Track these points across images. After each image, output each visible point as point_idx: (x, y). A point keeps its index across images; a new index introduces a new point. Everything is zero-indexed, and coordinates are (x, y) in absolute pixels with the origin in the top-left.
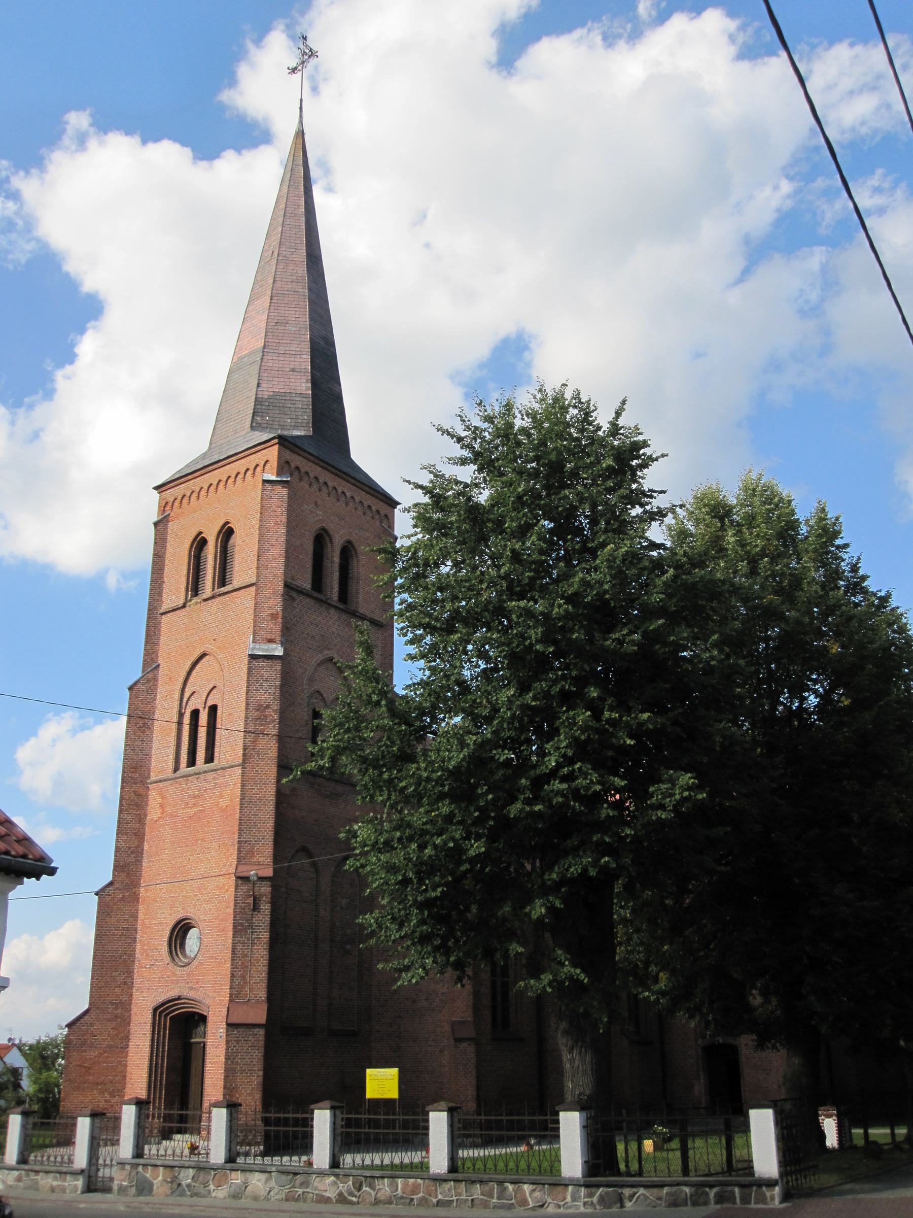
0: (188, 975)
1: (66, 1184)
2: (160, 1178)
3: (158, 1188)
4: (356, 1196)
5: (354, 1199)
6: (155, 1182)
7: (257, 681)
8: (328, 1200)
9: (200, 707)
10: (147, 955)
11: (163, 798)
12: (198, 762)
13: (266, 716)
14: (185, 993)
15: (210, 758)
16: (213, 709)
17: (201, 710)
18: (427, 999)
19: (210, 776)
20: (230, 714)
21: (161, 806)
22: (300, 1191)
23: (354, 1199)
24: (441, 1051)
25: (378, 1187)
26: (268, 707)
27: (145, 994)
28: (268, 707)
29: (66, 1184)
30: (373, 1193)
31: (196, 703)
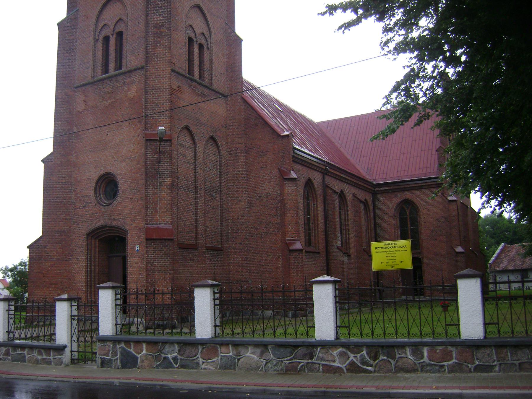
0: (111, 211)
1: (51, 358)
2: (144, 352)
3: (142, 361)
4: (371, 366)
5: (369, 368)
6: (139, 356)
7: (154, 8)
8: (337, 370)
9: (109, 34)
10: (80, 200)
11: (86, 96)
12: (110, 71)
13: (161, 32)
14: (109, 223)
15: (119, 66)
16: (120, 35)
17: (111, 36)
18: (266, 227)
19: (120, 78)
20: (133, 35)
21: (85, 101)
22: (304, 362)
23: (369, 368)
24: (277, 259)
25: (398, 356)
26: (163, 25)
27: (80, 226)
28: (163, 25)
29: (51, 358)
30: (393, 362)
31: (107, 32)
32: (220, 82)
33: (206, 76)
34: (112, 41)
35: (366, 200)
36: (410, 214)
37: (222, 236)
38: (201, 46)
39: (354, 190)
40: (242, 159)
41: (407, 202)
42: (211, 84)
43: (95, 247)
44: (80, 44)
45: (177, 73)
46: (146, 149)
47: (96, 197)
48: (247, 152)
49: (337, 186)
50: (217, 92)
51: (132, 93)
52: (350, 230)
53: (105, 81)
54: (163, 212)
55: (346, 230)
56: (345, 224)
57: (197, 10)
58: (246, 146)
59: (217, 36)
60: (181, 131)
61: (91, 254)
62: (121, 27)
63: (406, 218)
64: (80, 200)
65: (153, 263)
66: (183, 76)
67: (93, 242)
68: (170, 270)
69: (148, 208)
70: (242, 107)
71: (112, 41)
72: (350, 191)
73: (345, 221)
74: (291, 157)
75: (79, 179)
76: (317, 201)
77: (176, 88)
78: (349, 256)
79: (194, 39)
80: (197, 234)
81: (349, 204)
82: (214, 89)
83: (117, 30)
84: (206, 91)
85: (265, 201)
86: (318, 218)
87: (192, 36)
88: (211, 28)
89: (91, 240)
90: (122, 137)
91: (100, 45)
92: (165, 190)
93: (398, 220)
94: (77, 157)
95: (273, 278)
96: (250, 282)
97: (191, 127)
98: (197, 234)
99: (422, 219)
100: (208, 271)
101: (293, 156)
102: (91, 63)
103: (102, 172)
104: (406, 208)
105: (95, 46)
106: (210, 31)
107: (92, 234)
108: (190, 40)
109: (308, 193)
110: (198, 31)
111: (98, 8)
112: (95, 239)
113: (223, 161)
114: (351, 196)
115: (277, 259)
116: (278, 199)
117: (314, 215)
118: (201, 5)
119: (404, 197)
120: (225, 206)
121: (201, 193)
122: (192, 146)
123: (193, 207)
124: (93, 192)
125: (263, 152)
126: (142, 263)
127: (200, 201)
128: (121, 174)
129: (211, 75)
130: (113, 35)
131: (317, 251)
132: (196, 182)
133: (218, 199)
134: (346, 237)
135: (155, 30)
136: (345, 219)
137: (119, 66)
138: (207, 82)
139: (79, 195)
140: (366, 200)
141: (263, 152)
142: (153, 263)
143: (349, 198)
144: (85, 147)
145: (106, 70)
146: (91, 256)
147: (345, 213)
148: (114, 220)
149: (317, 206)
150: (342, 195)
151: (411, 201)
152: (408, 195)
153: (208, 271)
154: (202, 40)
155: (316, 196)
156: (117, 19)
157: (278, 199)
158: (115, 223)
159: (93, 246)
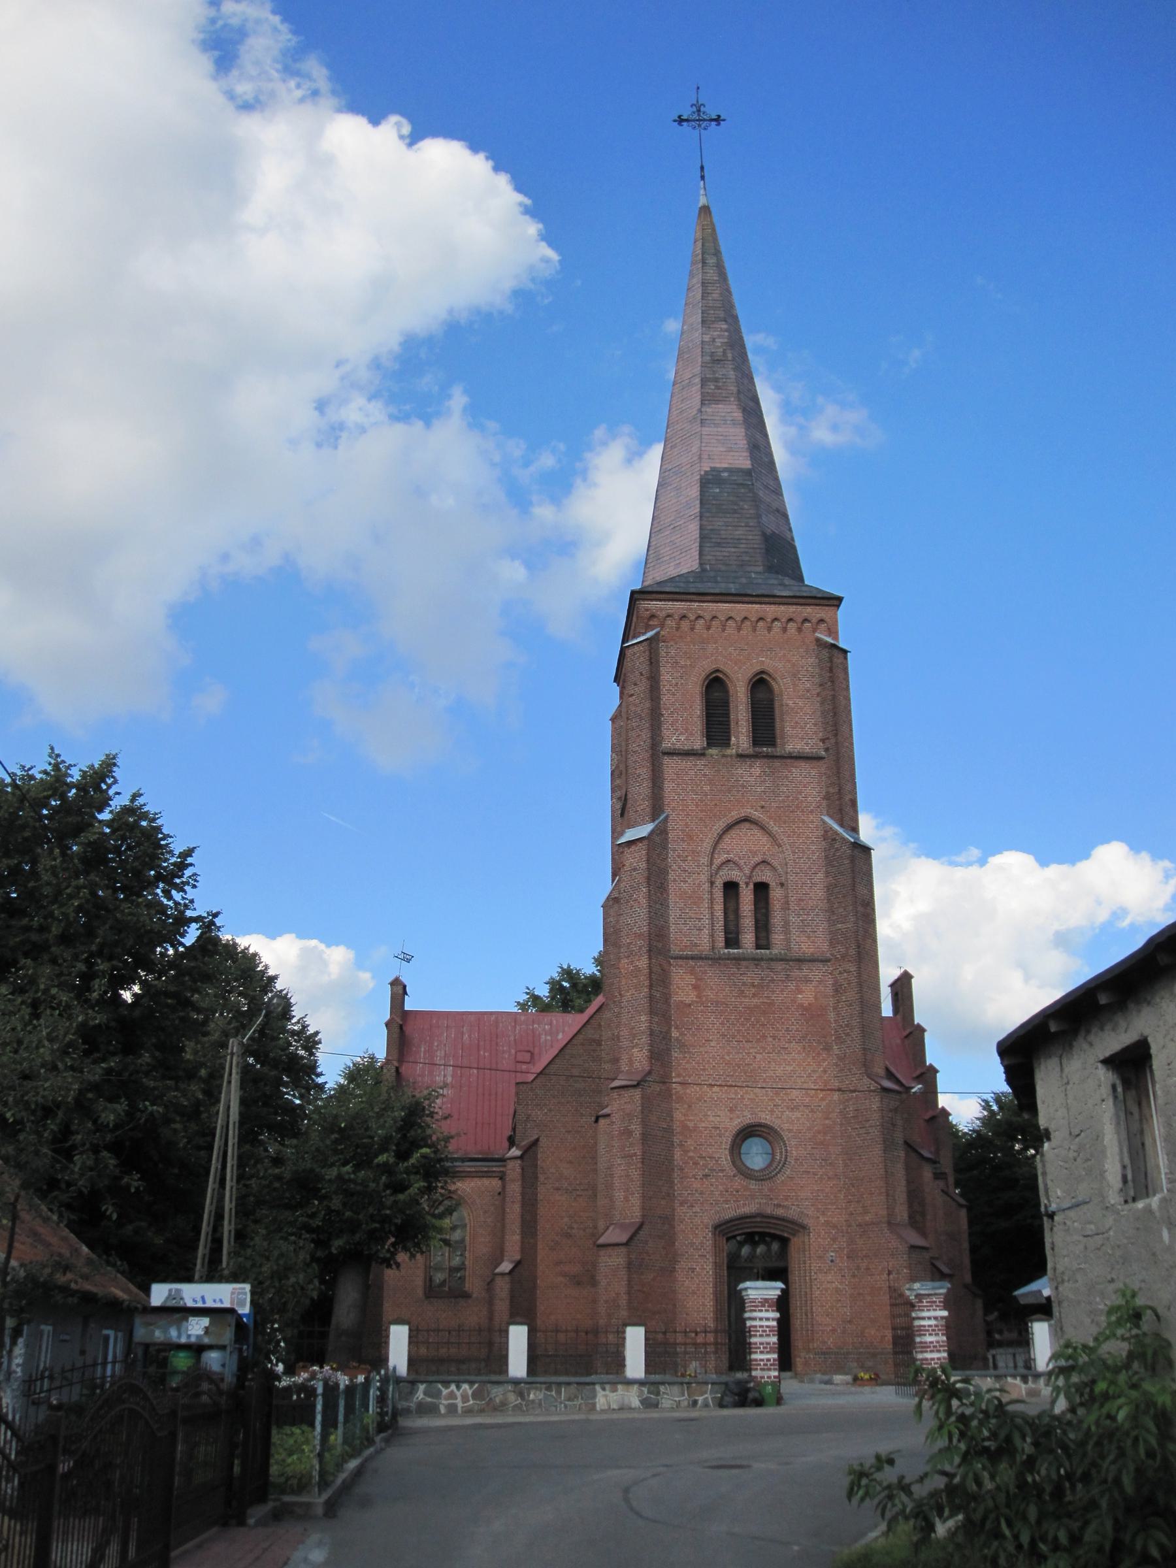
11: (698, 979)
14: (769, 1210)
16: (761, 889)
34: (747, 897)
44: (675, 880)
47: (734, 1163)
51: (807, 996)
53: (744, 963)
57: (747, 825)
62: (765, 876)
64: (696, 1164)
71: (747, 897)
75: (691, 1125)
90: (789, 1068)
107: (726, 1230)
124: (727, 1152)
126: (841, 1283)
128: (790, 1131)
130: (747, 884)
137: (763, 937)
139: (691, 1154)
144: (704, 1070)
145: (732, 940)
156: (757, 859)
158: (780, 1212)
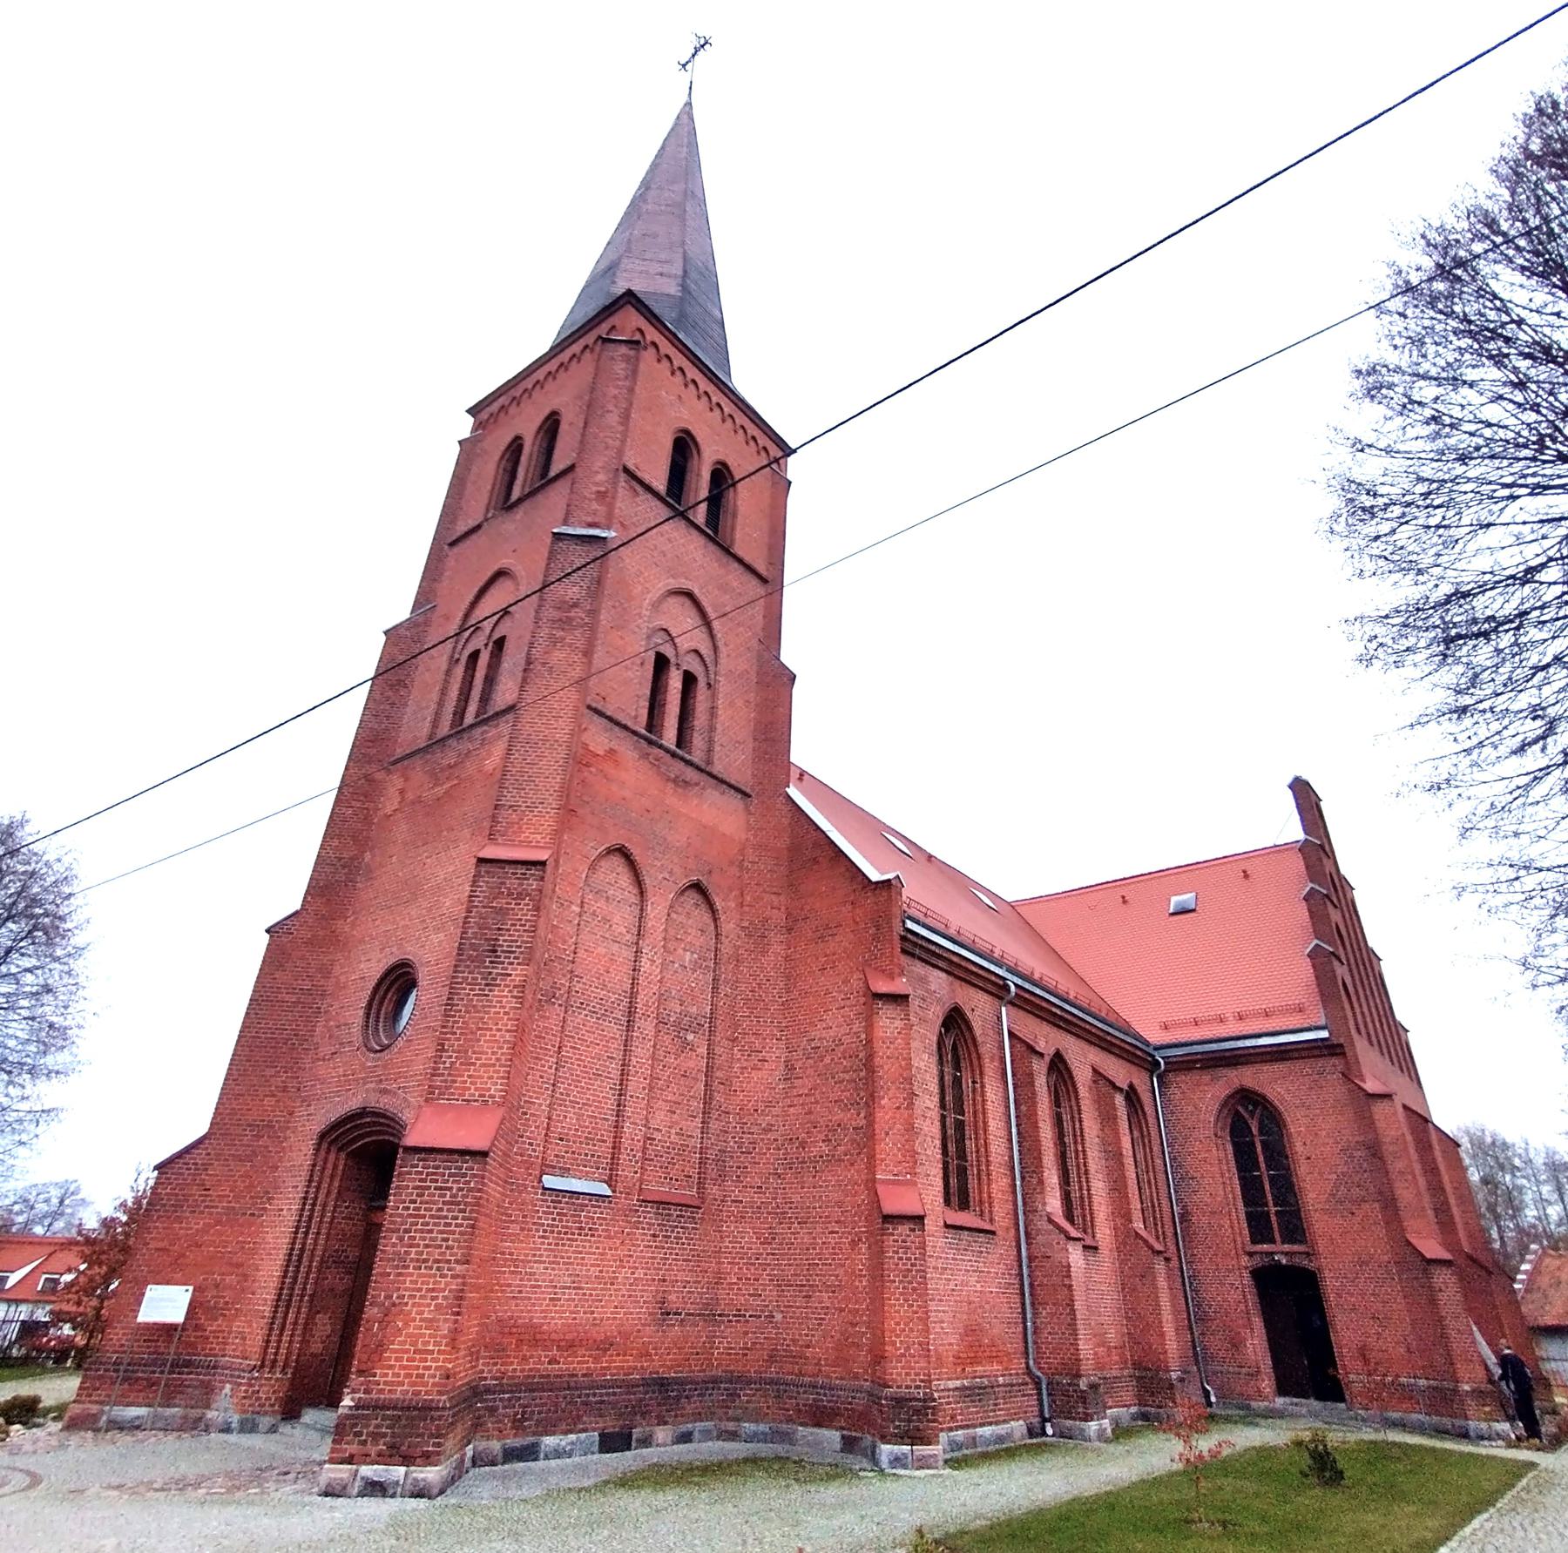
21: (402, 792)
24: (854, 1244)
26: (575, 605)
31: (478, 642)
32: (734, 759)
33: (698, 741)
34: (484, 658)
35: (1131, 1086)
36: (1261, 1133)
37: (702, 1162)
38: (689, 680)
39: (1095, 1056)
40: (778, 948)
41: (1246, 1098)
42: (709, 762)
43: (332, 1177)
45: (610, 719)
46: (474, 883)
48: (790, 930)
49: (1047, 1039)
50: (723, 782)
52: (1092, 1167)
54: (484, 1065)
55: (1078, 1166)
56: (1077, 1151)
57: (688, 602)
58: (789, 915)
59: (735, 660)
60: (600, 857)
61: (316, 1198)
63: (1253, 1144)
65: (406, 1231)
66: (635, 733)
67: (332, 1157)
68: (457, 1262)
69: (443, 1050)
70: (786, 821)
72: (1083, 1059)
73: (1076, 1143)
74: (897, 938)
76: (981, 1073)
77: (601, 753)
78: (1091, 1249)
79: (673, 660)
80: (616, 1147)
81: (1083, 1092)
82: (715, 772)
83: (496, 636)
84: (691, 774)
85: (827, 1060)
86: (985, 1123)
87: (668, 651)
88: (720, 644)
89: (328, 1152)
91: (459, 671)
92: (503, 999)
93: (1230, 1148)
94: (353, 925)
95: (842, 1310)
96: (778, 1317)
97: (636, 853)
98: (616, 1147)
99: (1299, 1147)
100: (640, 1273)
101: (903, 938)
102: (433, 706)
103: (392, 960)
104: (1246, 1116)
105: (448, 672)
106: (715, 648)
108: (661, 663)
109: (955, 1048)
110: (684, 644)
111: (471, 597)
112: (340, 1150)
113: (726, 949)
114: (1089, 1073)
115: (854, 1244)
116: (861, 1055)
117: (975, 1112)
118: (696, 591)
119: (1236, 1084)
120: (718, 1074)
121: (645, 1027)
122: (635, 900)
123: (614, 1069)
124: (361, 1013)
125: (828, 927)
127: (641, 1053)
129: (711, 741)
131: (987, 1227)
132: (633, 995)
133: (703, 1050)
134: (1081, 1189)
135: (556, 614)
136: (1075, 1136)
138: (697, 756)
140: (1131, 1086)
141: (828, 927)
142: (406, 1231)
143: (1082, 1076)
146: (314, 1205)
147: (1073, 1117)
148: (385, 1091)
149: (983, 1086)
150: (1059, 1066)
151: (1255, 1093)
152: (1247, 1077)
153: (640, 1273)
154: (695, 667)
155: (979, 1058)
157: (861, 1055)
159: (328, 1172)
